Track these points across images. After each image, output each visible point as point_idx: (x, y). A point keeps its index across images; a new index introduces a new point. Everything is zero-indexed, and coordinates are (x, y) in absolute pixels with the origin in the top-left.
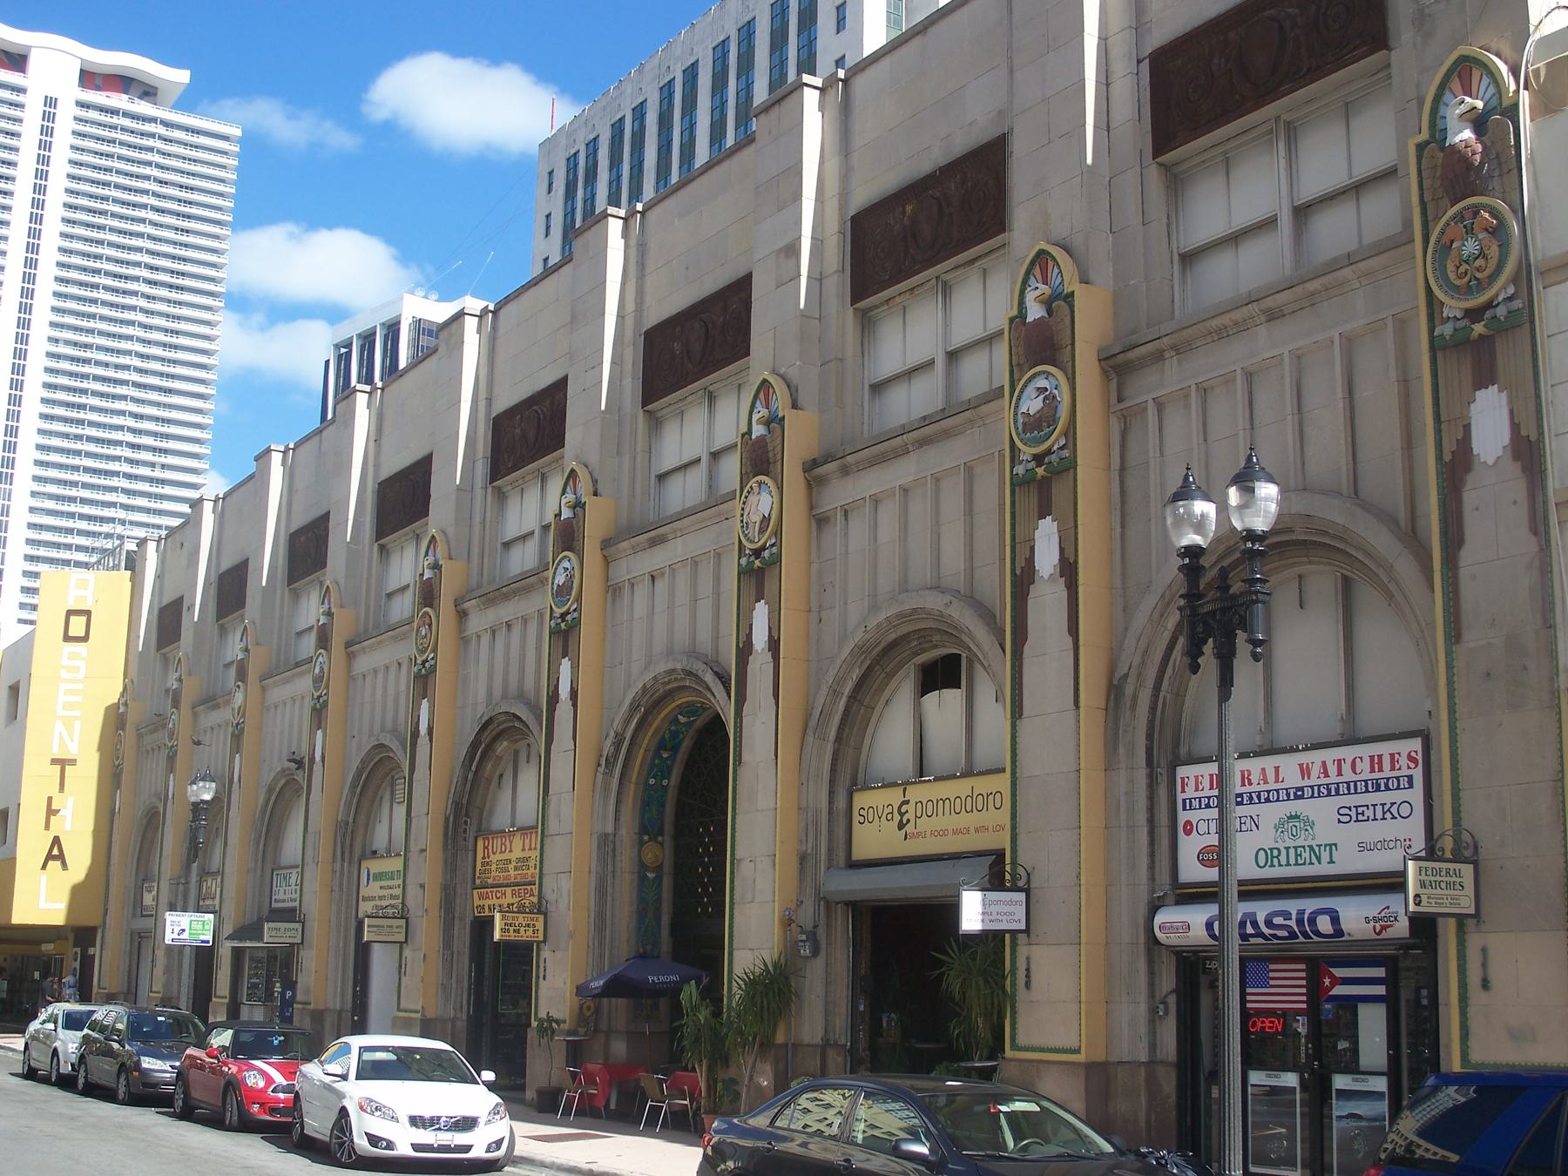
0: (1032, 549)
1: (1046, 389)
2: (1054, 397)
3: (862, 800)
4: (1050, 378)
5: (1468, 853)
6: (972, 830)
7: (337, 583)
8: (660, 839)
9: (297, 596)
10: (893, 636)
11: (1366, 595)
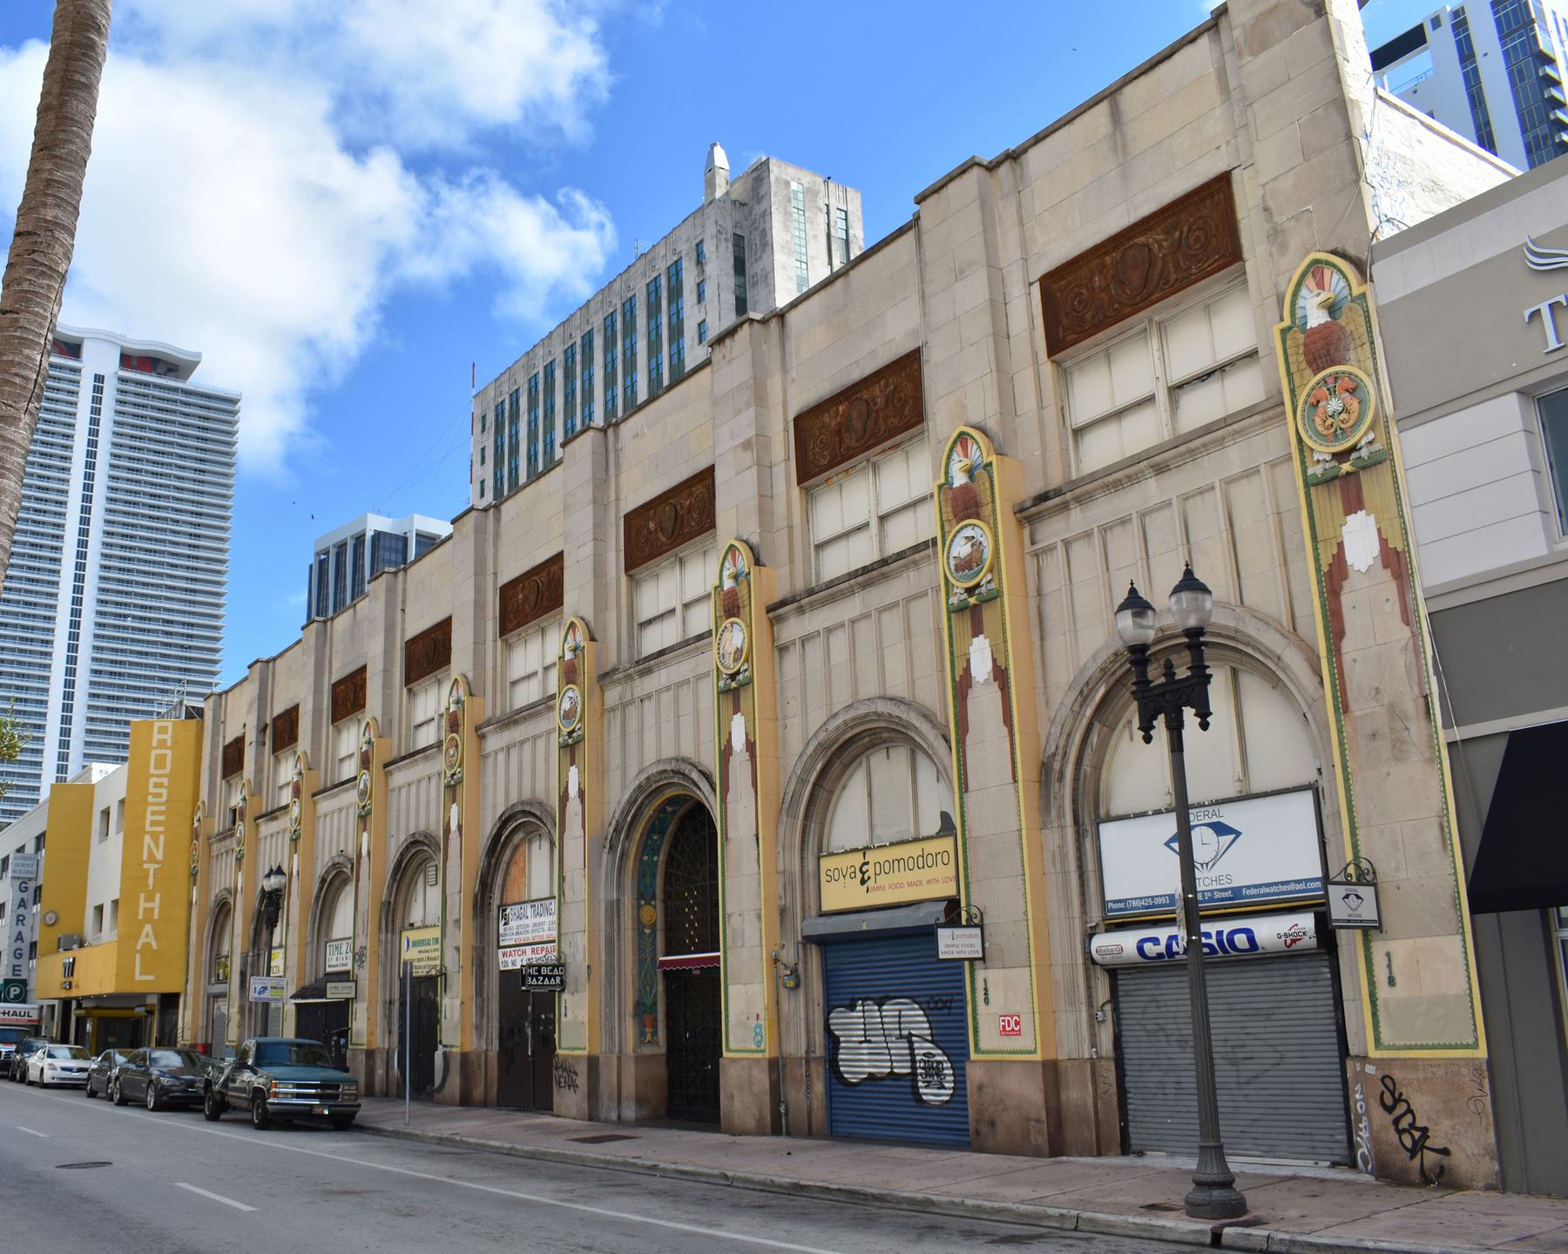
0: (968, 661)
1: (973, 538)
2: (980, 543)
3: (826, 864)
4: (976, 529)
6: (925, 882)
7: (375, 719)
8: (653, 903)
9: (1065, 370)
10: (849, 735)
11: (921, 757)
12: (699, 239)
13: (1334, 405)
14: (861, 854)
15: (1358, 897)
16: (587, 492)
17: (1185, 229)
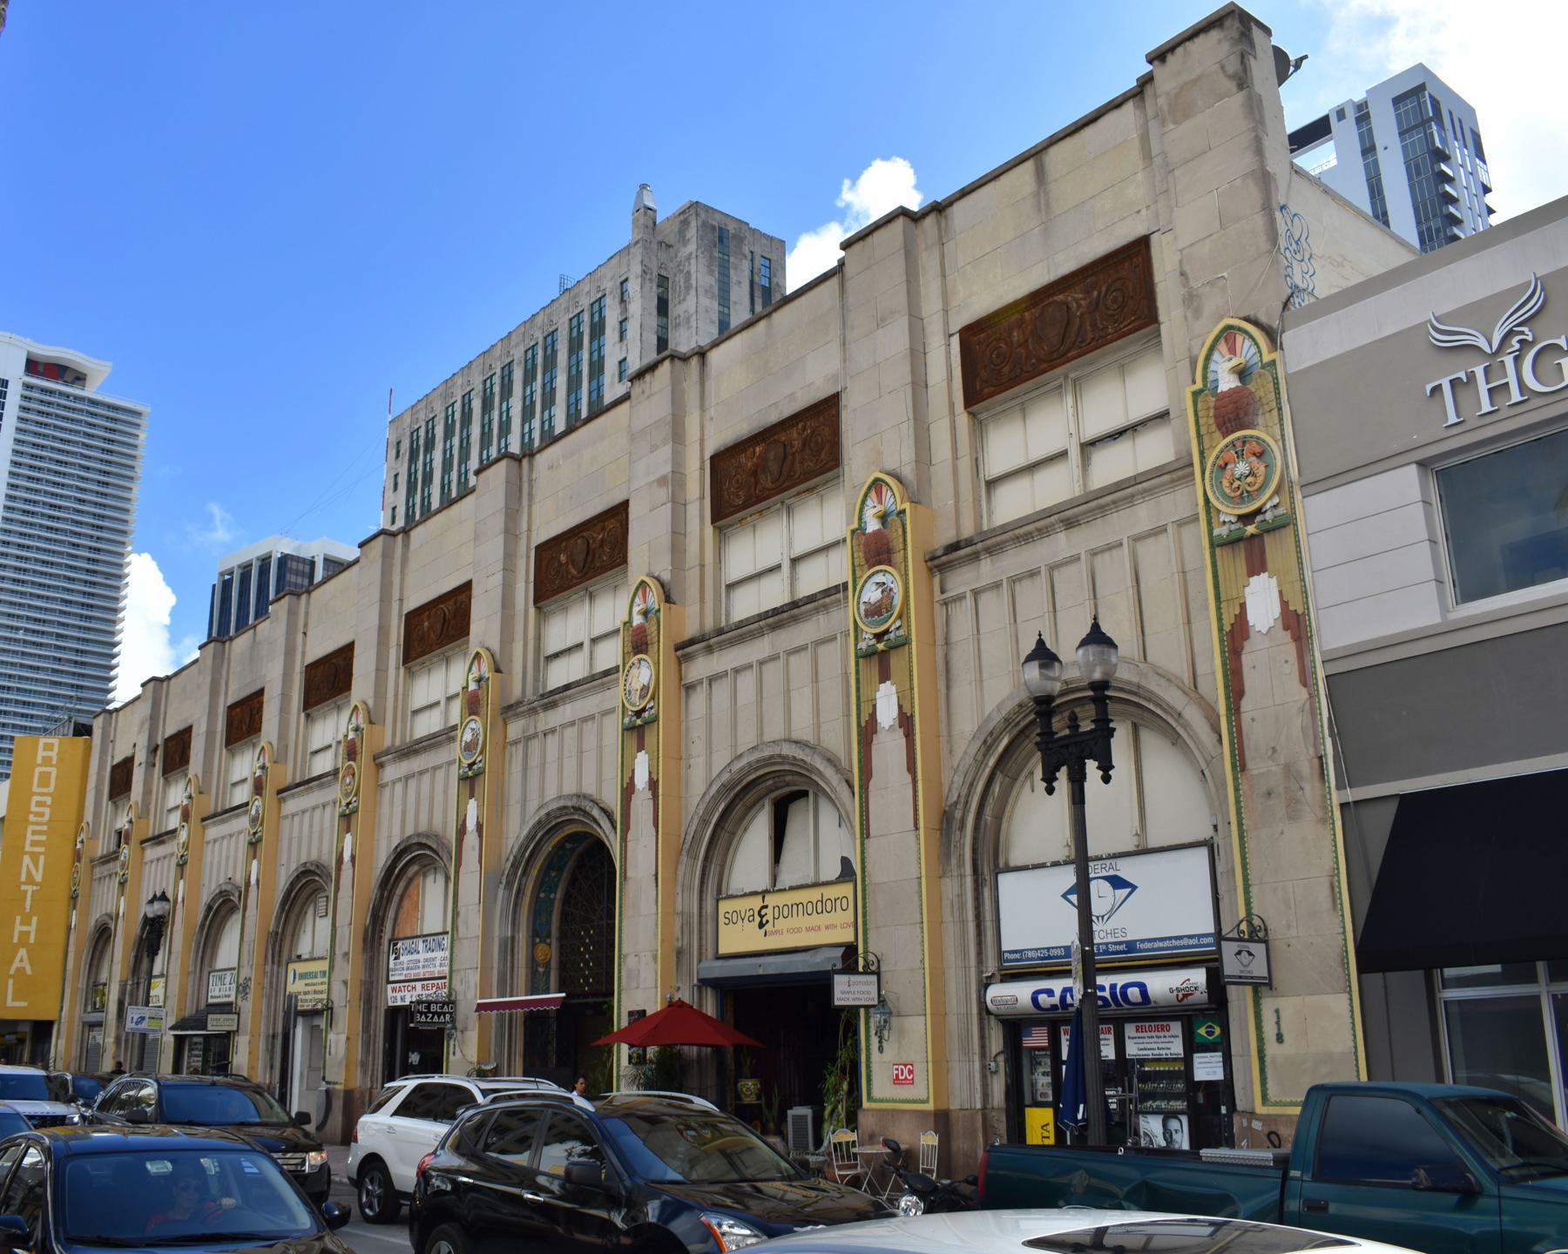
0: (874, 706)
1: (884, 584)
3: (724, 906)
4: (887, 575)
5: (1261, 935)
7: (271, 744)
8: (548, 941)
12: (623, 278)
13: (1241, 468)
14: (760, 898)
15: (1250, 954)
16: (499, 522)
17: (1104, 289)
